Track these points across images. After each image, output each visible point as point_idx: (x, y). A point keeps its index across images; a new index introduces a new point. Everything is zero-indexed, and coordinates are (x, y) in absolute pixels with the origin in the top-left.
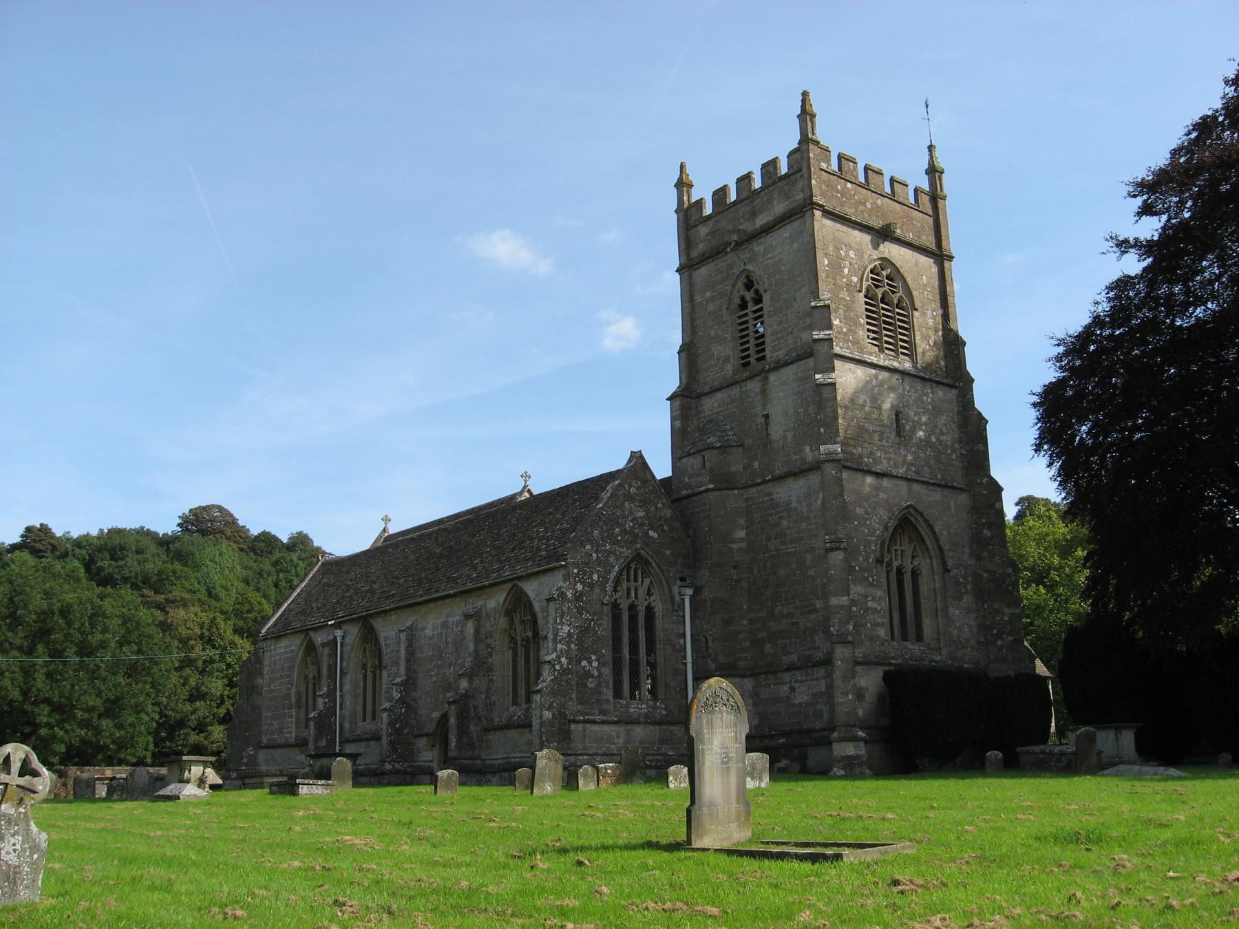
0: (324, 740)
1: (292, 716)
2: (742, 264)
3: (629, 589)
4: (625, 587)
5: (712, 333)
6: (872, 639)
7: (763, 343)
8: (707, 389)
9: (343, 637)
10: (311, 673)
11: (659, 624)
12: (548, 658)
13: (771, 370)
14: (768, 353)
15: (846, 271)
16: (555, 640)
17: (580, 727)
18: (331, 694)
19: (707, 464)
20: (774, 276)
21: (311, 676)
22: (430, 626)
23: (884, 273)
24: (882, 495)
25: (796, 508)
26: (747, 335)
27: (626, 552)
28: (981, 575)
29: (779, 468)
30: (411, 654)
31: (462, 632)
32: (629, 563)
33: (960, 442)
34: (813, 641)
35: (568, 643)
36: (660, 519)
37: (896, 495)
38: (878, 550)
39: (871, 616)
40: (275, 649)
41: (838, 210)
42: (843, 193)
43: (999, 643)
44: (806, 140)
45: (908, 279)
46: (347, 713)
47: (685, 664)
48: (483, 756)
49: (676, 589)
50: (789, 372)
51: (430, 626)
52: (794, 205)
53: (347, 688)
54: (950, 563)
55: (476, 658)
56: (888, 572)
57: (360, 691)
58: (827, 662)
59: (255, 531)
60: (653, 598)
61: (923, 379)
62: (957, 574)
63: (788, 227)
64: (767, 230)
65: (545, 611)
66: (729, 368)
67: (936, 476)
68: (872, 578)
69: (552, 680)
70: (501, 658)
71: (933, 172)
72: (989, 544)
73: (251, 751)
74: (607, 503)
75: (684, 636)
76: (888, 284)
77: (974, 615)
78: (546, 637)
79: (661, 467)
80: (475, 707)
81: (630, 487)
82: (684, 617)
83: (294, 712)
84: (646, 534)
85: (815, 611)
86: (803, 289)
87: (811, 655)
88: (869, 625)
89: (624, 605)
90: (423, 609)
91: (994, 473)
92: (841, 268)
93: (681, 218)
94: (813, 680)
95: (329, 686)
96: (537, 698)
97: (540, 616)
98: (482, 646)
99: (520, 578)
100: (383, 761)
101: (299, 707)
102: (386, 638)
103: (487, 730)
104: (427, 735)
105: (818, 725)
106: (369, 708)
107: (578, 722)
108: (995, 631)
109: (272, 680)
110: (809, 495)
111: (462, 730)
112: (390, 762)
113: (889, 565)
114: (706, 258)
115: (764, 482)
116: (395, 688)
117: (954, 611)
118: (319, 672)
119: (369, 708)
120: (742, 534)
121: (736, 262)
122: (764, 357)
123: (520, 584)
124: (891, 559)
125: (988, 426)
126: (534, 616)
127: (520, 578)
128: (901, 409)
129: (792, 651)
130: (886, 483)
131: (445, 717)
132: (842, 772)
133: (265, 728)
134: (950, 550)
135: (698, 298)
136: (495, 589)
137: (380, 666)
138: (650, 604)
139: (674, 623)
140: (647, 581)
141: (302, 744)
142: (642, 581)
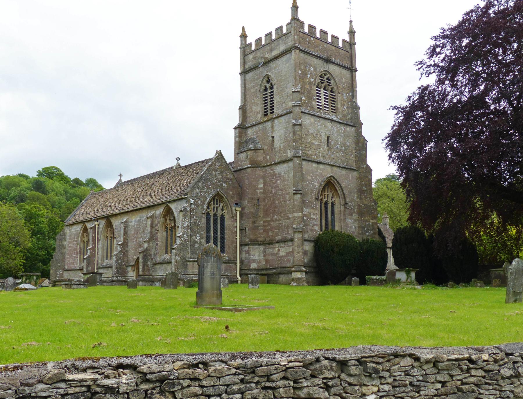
0: (90, 267)
1: (78, 258)
2: (266, 72)
3: (214, 208)
4: (212, 207)
5: (253, 101)
6: (312, 230)
7: (273, 106)
8: (249, 125)
9: (99, 225)
10: (86, 239)
11: (227, 222)
12: (179, 235)
13: (276, 118)
14: (275, 111)
15: (309, 76)
16: (182, 228)
17: (191, 263)
18: (93, 248)
19: (249, 157)
20: (278, 78)
21: (85, 241)
22: (133, 221)
23: (326, 77)
24: (319, 171)
25: (283, 176)
26: (267, 103)
27: (214, 193)
28: (361, 206)
29: (278, 159)
30: (126, 232)
31: (146, 224)
32: (214, 197)
33: (355, 150)
34: (288, 231)
35: (187, 229)
36: (228, 179)
37: (327, 172)
38: (317, 194)
39: (312, 221)
40: (71, 230)
41: (307, 50)
42: (309, 42)
43: (367, 234)
44: (295, 19)
45: (337, 80)
46: (100, 256)
47: (237, 239)
48: (153, 274)
49: (234, 208)
50: (282, 119)
51: (133, 221)
52: (287, 47)
53: (100, 246)
54: (348, 200)
55: (151, 234)
56: (321, 203)
57: (105, 247)
58: (292, 240)
59: (72, 178)
60: (224, 211)
61: (340, 123)
62: (351, 205)
63: (285, 56)
64: (277, 58)
65: (178, 216)
66: (259, 116)
67: (344, 164)
68: (313, 205)
69: (180, 244)
70: (161, 235)
71: (352, 33)
72: (365, 193)
73: (61, 272)
74: (205, 172)
75: (236, 227)
76: (327, 82)
77: (357, 222)
78: (178, 227)
79: (230, 157)
80: (150, 255)
81: (215, 165)
82: (237, 219)
83: (78, 256)
84: (222, 185)
85: (289, 218)
86: (290, 84)
87: (287, 236)
88: (311, 225)
89: (212, 214)
90: (131, 214)
91: (369, 163)
92: (306, 75)
93: (242, 51)
94: (287, 246)
95: (92, 245)
96: (174, 251)
97: (176, 218)
98: (154, 230)
99: (169, 202)
100: (113, 276)
101: (81, 254)
102: (116, 226)
103: (155, 264)
104: (132, 266)
105: (288, 265)
106: (109, 255)
107: (190, 261)
108: (366, 229)
109: (70, 242)
110: (289, 170)
111: (144, 264)
112: (116, 276)
113: (321, 200)
114: (251, 69)
115: (271, 165)
116: (119, 246)
117: (349, 220)
118: (89, 239)
119: (109, 255)
120: (261, 186)
121: (262, 72)
122: (273, 112)
123: (169, 204)
124: (322, 198)
125: (367, 144)
126: (174, 218)
127: (169, 202)
128: (330, 136)
129: (280, 234)
130: (321, 166)
131: (138, 258)
132: (295, 284)
133: (67, 262)
134: (348, 195)
135: (247, 86)
136: (159, 206)
137: (113, 238)
138: (223, 214)
139: (233, 222)
140: (222, 205)
141: (81, 269)
142: (220, 205)
